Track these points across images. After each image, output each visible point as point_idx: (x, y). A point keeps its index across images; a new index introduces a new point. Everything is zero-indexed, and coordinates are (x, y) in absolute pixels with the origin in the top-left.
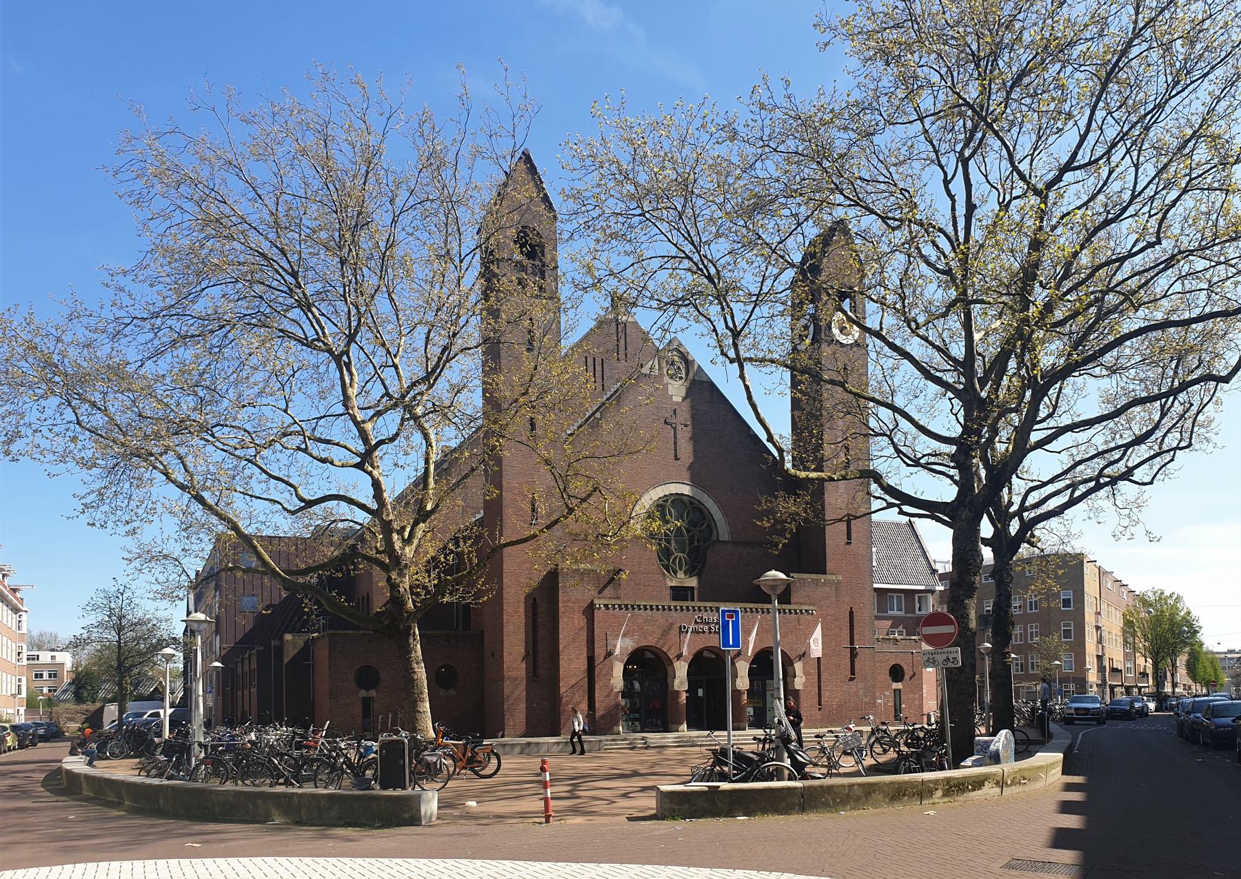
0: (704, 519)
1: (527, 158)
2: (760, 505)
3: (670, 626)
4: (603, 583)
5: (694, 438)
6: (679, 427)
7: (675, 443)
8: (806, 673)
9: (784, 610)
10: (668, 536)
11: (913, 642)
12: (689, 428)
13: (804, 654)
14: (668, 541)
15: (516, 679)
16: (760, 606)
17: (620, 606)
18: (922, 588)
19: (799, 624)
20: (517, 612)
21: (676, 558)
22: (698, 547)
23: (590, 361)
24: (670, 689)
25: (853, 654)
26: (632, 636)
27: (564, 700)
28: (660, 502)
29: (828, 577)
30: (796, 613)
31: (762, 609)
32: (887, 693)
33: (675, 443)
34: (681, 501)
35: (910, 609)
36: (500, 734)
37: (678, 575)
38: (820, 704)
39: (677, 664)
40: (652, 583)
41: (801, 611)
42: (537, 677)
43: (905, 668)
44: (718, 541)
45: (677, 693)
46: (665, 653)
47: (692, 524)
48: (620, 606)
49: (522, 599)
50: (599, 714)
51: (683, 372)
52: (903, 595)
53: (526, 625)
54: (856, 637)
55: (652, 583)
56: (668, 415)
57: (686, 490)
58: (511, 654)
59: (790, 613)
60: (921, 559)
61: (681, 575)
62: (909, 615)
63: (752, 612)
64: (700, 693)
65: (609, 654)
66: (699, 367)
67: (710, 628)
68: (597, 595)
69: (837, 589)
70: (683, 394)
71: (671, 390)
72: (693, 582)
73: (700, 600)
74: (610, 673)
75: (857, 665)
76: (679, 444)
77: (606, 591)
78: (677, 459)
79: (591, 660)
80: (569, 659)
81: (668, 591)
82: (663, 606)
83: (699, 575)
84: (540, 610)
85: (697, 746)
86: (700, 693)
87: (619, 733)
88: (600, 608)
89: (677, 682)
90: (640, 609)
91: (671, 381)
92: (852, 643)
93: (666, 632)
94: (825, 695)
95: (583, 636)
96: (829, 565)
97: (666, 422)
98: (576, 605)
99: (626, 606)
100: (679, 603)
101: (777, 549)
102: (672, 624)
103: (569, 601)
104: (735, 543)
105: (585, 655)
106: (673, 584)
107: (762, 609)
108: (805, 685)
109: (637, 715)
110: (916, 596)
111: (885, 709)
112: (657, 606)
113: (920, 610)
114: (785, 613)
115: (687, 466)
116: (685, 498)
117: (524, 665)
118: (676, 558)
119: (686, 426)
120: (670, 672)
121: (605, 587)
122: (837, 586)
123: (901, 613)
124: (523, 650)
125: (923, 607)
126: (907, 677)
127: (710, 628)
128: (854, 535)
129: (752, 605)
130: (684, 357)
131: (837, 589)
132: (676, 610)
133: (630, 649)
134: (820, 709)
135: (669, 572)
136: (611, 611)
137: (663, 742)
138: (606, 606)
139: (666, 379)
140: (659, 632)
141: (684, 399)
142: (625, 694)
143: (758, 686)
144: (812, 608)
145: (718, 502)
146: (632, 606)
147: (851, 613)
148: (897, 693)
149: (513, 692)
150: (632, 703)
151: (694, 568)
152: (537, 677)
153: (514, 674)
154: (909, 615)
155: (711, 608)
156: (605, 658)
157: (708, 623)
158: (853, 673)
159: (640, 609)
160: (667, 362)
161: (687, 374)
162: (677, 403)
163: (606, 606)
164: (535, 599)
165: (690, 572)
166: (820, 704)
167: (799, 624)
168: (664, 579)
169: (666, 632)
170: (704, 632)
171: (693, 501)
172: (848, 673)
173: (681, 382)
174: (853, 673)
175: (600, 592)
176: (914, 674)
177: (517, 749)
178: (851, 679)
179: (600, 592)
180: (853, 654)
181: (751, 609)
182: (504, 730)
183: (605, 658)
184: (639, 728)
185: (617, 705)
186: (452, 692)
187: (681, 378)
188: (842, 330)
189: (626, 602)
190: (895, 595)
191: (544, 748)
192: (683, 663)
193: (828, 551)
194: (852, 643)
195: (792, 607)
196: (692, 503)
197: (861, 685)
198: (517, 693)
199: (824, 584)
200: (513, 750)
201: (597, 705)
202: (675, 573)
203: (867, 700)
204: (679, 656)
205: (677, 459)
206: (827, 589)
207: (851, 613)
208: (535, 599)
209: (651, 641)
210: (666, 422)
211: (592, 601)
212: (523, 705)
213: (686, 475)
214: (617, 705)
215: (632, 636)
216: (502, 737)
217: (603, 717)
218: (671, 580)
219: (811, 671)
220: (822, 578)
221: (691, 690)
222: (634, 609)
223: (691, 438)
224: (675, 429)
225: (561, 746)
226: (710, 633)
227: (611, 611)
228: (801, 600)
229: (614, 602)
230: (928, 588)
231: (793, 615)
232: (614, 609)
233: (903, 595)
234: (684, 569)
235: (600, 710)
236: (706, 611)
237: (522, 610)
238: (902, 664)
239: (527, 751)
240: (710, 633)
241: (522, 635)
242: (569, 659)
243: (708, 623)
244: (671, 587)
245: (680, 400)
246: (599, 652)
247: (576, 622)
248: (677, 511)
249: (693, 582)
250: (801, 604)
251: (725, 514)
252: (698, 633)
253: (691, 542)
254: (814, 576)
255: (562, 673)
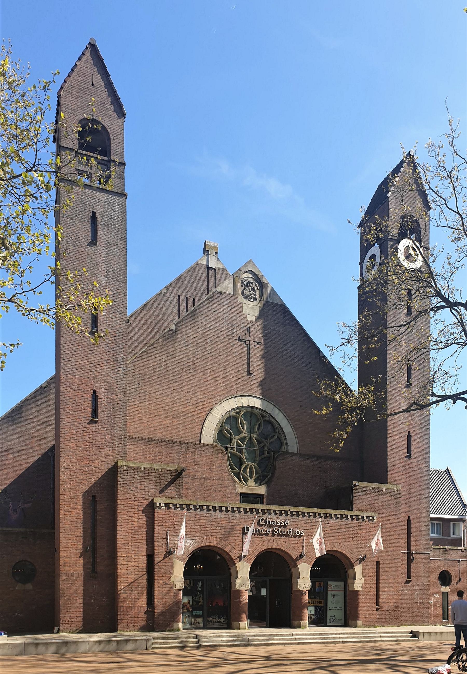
0: (275, 431)
1: (93, 47)
2: (318, 390)
3: (232, 529)
4: (165, 482)
5: (266, 357)
6: (252, 345)
7: (248, 359)
8: (365, 576)
9: (346, 516)
10: (240, 445)
11: (460, 552)
12: (261, 346)
13: (364, 558)
14: (240, 451)
15: (73, 574)
16: (323, 511)
17: (181, 505)
18: (456, 517)
19: (360, 529)
20: (75, 509)
21: (246, 467)
22: (269, 458)
23: (183, 300)
24: (233, 589)
25: (410, 559)
26: (194, 536)
27: (122, 597)
28: (233, 413)
29: (389, 486)
30: (358, 519)
31: (325, 514)
32: (437, 596)
33: (248, 359)
34: (253, 414)
35: (447, 533)
36: (56, 629)
37: (249, 483)
38: (378, 605)
39: (239, 565)
40: (223, 490)
41: (362, 517)
42: (96, 573)
43: (452, 573)
44: (287, 453)
45: (239, 593)
46: (228, 554)
47: (263, 437)
48: (181, 505)
49: (80, 495)
50: (157, 611)
51: (258, 293)
52: (441, 523)
53: (84, 521)
54: (413, 544)
55: (223, 490)
56: (242, 333)
57: (257, 403)
58: (67, 550)
59: (352, 519)
60: (456, 497)
61: (251, 482)
62: (446, 538)
63: (315, 516)
64: (264, 592)
65: (169, 553)
66: (273, 289)
67: (273, 531)
68: (157, 494)
69: (397, 498)
70: (257, 313)
71: (245, 309)
72: (262, 490)
73: (268, 503)
74: (170, 572)
75: (413, 569)
76: (252, 360)
77: (169, 491)
78: (249, 374)
79: (150, 558)
80: (128, 557)
81: (239, 497)
82: (226, 508)
83: (268, 484)
84: (100, 507)
85: (252, 645)
86: (264, 592)
87: (178, 630)
88: (160, 508)
89: (238, 581)
90: (202, 510)
91: (245, 301)
92: (409, 548)
93: (230, 531)
94: (383, 596)
95: (143, 534)
96: (390, 476)
97: (240, 339)
98: (136, 503)
99: (188, 506)
100: (248, 506)
101: (338, 446)
102: (235, 525)
103: (128, 499)
104: (302, 455)
105: (144, 553)
106: (244, 490)
107: (325, 514)
108: (364, 586)
109: (200, 613)
110: (452, 523)
111: (435, 609)
112: (220, 507)
113: (453, 534)
114: (347, 518)
115: (259, 381)
116: (257, 411)
117: (81, 561)
118: (246, 467)
119: (259, 344)
120: (233, 573)
121: (167, 486)
122: (397, 495)
123: (440, 536)
124: (81, 547)
125: (456, 531)
126: (454, 582)
127: (273, 531)
128: (413, 450)
129: (315, 510)
130: (258, 279)
131: (397, 498)
132: (240, 512)
133: (192, 549)
134: (377, 609)
135: (239, 479)
136: (172, 510)
137: (218, 641)
138: (167, 505)
139: (241, 299)
140: (221, 532)
141: (258, 319)
142: (186, 592)
143: (320, 586)
144: (373, 514)
145: (288, 417)
146: (195, 506)
147: (409, 521)
148: (445, 595)
149: (69, 587)
150: (196, 601)
151: (265, 477)
152: (96, 573)
153: (71, 570)
154: (446, 538)
155: (275, 511)
156: (165, 557)
157: (271, 526)
158: (409, 576)
159: (202, 510)
160: (243, 282)
161: (261, 296)
162: (251, 322)
163: (167, 505)
164: (94, 497)
165: (259, 481)
166: (378, 605)
167: (360, 529)
168: (235, 486)
169: (230, 531)
170: (267, 534)
171: (265, 414)
172: (405, 576)
173: (255, 303)
174: (409, 576)
175: (161, 492)
176: (460, 579)
177: (52, 649)
178: (408, 582)
179: (161, 492)
180: (410, 559)
181: (314, 514)
182: (59, 625)
183: (165, 557)
184: (201, 625)
185: (177, 603)
186: (29, 586)
187: (255, 299)
188: (408, 257)
189: (188, 502)
190: (436, 522)
191: (84, 647)
192: (245, 563)
193: (389, 463)
194: (409, 548)
195: (354, 513)
196: (263, 416)
197: (416, 588)
198: (74, 588)
199: (385, 493)
200: (47, 649)
201: (156, 602)
202: (246, 480)
203: (421, 601)
204: (241, 558)
205: (249, 374)
206: (388, 497)
207: (409, 521)
208: (94, 497)
209: (213, 542)
210: (240, 339)
211: (153, 500)
212: (80, 601)
213: (257, 391)
214: (177, 603)
215: (194, 536)
216: (58, 632)
217: (162, 614)
218: (242, 487)
219: (370, 573)
220: (383, 487)
221: (256, 588)
222: (196, 509)
223: (263, 357)
224: (248, 346)
225: (103, 645)
226: (273, 535)
227: (172, 510)
228: (363, 507)
229: (175, 501)
230: (461, 517)
231: (355, 521)
232: (176, 508)
233: (441, 523)
234: (254, 477)
235: (159, 608)
236: (270, 514)
237: (80, 506)
238: (450, 570)
239: (64, 650)
240: (273, 535)
241: (80, 531)
242: (128, 557)
243: (271, 526)
244: (241, 494)
245: (254, 319)
246: (159, 551)
247: (136, 520)
248: (249, 423)
249: (262, 490)
250: (363, 511)
251: (295, 428)
252: (261, 535)
253: (262, 453)
254: (376, 485)
255: (120, 569)
